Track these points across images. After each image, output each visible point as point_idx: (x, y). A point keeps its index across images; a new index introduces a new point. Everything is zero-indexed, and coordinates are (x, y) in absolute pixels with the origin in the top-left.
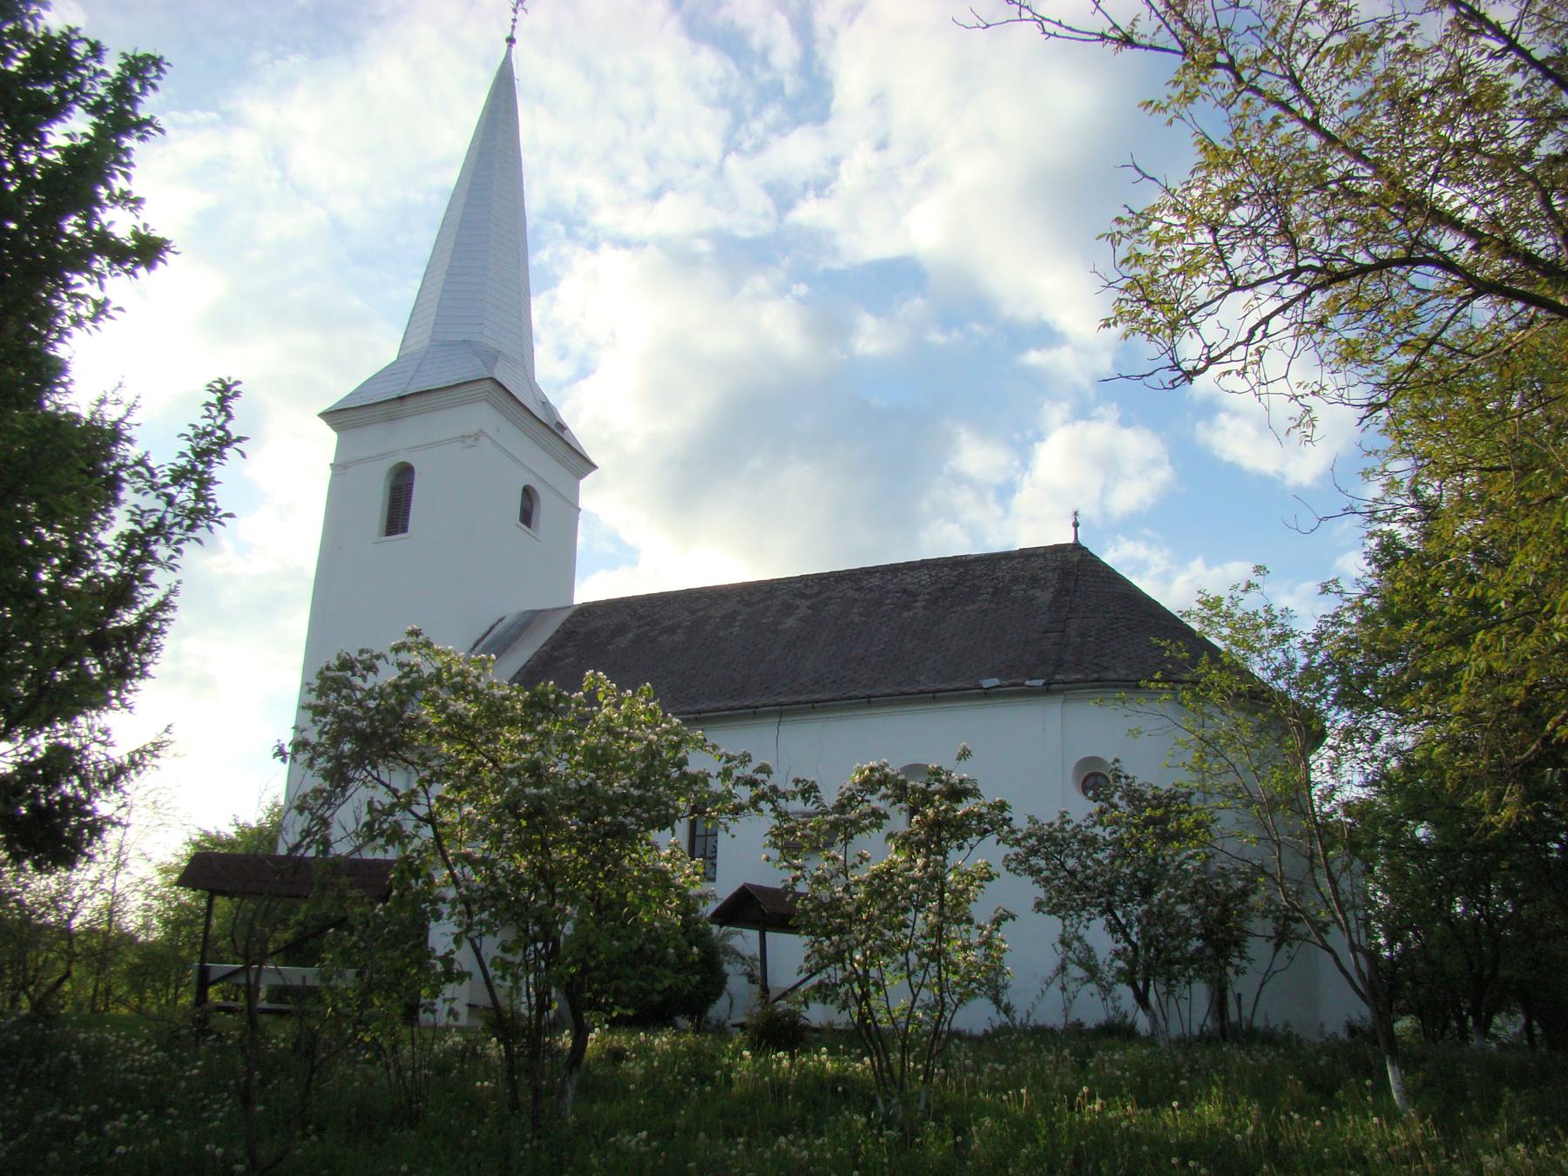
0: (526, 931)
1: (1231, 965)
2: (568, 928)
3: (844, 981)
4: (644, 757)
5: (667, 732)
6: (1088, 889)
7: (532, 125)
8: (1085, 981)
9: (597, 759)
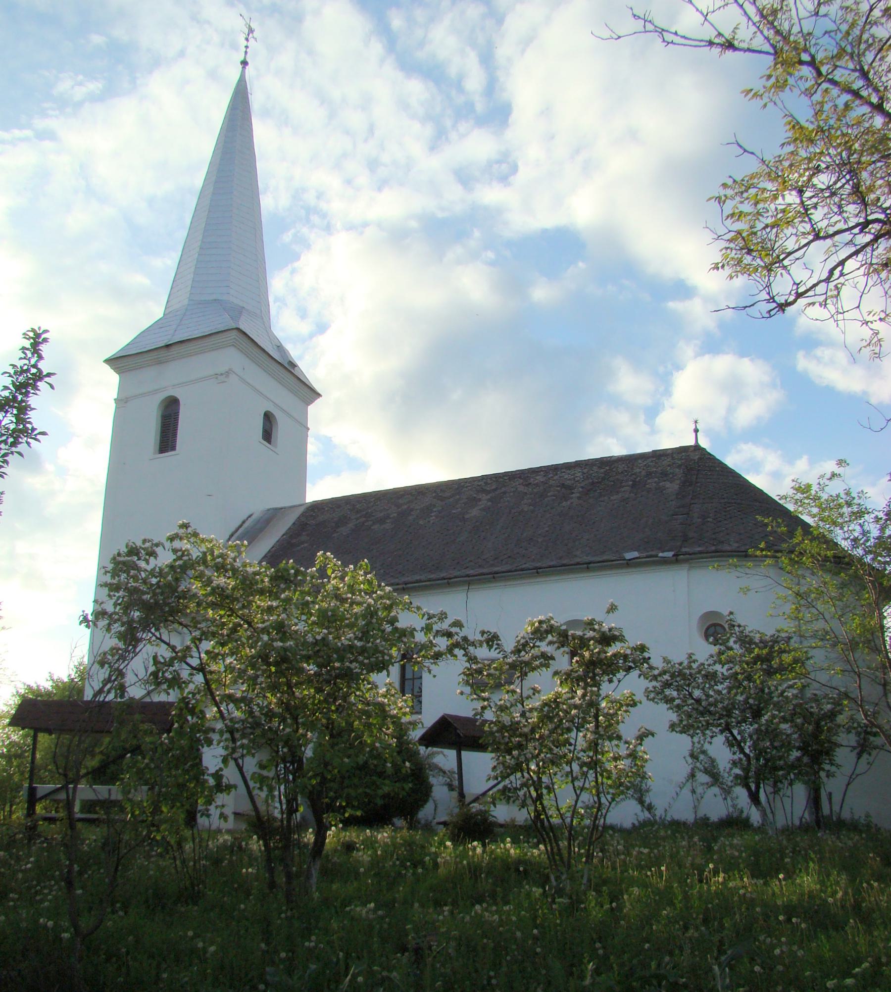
0: (278, 752)
1: (823, 769)
2: (309, 752)
3: (524, 785)
4: (364, 616)
5: (381, 597)
6: (710, 713)
7: (263, 133)
9: (328, 619)
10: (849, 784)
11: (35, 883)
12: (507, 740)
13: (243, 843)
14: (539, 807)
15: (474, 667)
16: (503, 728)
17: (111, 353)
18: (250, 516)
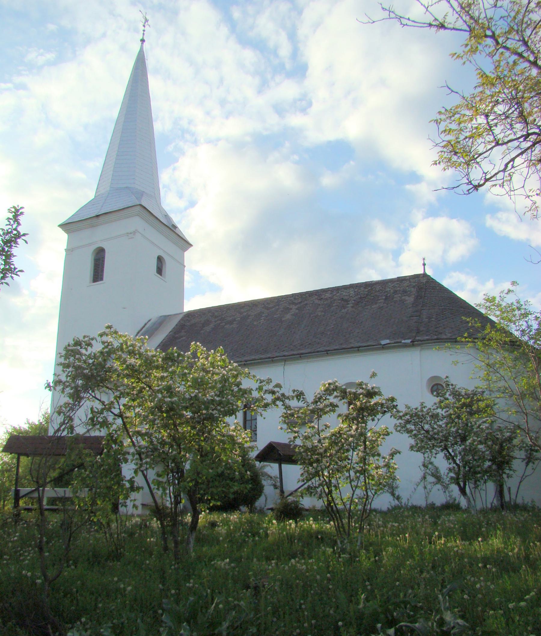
0: (168, 466)
1: (505, 473)
3: (320, 485)
4: (221, 382)
5: (231, 370)
6: (435, 439)
7: (155, 84)
8: (435, 484)
9: (199, 384)
10: (521, 482)
11: (19, 549)
12: (309, 457)
13: (148, 523)
14: (330, 498)
15: (289, 412)
16: (307, 450)
17: (61, 221)
18: (149, 321)
